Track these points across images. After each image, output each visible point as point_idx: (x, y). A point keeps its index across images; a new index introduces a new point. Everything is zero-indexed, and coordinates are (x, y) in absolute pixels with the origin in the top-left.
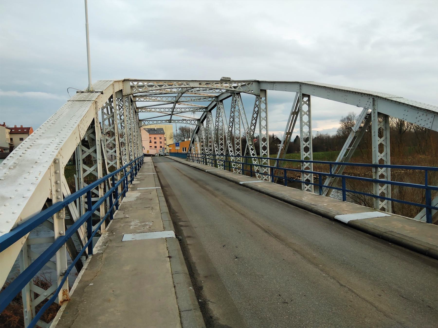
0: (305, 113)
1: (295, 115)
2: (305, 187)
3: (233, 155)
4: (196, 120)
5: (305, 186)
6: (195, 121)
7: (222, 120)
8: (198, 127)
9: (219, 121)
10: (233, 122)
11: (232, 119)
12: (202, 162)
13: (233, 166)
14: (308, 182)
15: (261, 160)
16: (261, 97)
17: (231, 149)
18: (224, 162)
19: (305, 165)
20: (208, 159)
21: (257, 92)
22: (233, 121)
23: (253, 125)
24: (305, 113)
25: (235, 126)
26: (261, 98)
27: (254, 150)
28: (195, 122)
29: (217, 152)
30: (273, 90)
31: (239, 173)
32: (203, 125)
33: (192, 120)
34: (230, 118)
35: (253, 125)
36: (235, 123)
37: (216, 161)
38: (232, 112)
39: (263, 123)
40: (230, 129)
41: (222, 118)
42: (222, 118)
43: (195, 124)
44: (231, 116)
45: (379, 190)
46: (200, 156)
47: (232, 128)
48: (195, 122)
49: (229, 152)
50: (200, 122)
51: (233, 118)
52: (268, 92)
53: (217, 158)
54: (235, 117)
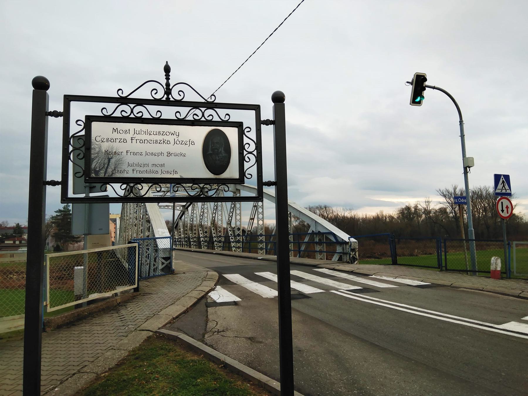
0: (260, 207)
1: (6, 242)
2: (260, 252)
3: (203, 236)
4: (181, 206)
5: (260, 251)
6: (180, 207)
7: (207, 207)
8: (182, 212)
9: (204, 207)
10: (234, 208)
11: (215, 208)
12: (179, 245)
13: (215, 245)
14: (262, 249)
15: (236, 238)
16: (236, 193)
17: (201, 232)
18: (208, 244)
19: (260, 238)
20: (192, 242)
21: (235, 190)
22: (216, 208)
23: (231, 213)
24: (260, 207)
25: (236, 211)
26: (237, 195)
27: (215, 230)
28: (180, 208)
29: (202, 235)
30: (243, 190)
31: (220, 250)
32: (188, 211)
33: (177, 206)
34: (201, 209)
35: (231, 213)
36: (218, 211)
37: (190, 242)
38: (203, 205)
39: (238, 212)
40: (214, 215)
41: (207, 205)
42: (207, 205)
43: (180, 209)
44: (202, 207)
45: (261, 246)
46: (183, 240)
47: (215, 214)
48: (180, 208)
49: (212, 234)
50: (185, 207)
51: (217, 207)
52: (241, 191)
53: (201, 240)
54: (205, 209)
